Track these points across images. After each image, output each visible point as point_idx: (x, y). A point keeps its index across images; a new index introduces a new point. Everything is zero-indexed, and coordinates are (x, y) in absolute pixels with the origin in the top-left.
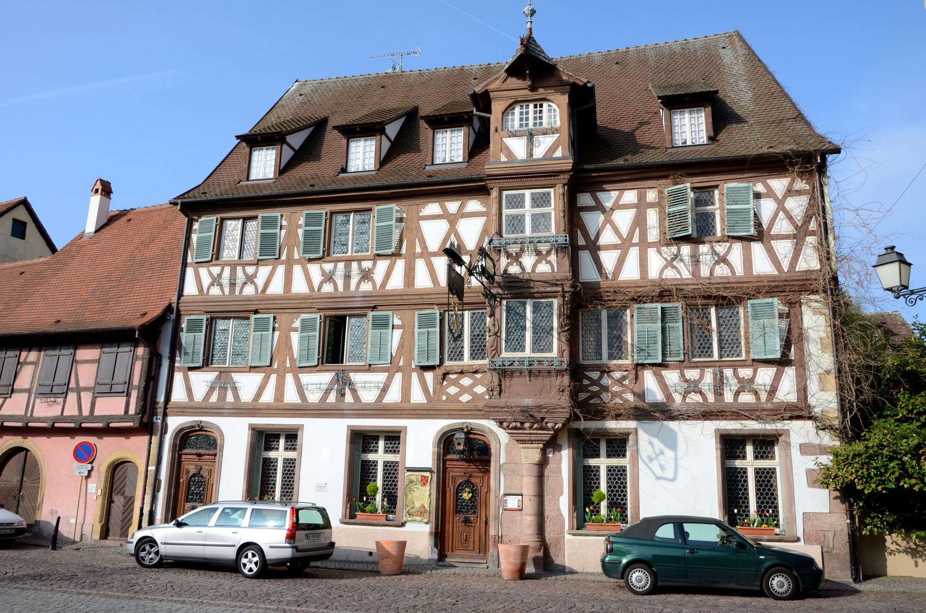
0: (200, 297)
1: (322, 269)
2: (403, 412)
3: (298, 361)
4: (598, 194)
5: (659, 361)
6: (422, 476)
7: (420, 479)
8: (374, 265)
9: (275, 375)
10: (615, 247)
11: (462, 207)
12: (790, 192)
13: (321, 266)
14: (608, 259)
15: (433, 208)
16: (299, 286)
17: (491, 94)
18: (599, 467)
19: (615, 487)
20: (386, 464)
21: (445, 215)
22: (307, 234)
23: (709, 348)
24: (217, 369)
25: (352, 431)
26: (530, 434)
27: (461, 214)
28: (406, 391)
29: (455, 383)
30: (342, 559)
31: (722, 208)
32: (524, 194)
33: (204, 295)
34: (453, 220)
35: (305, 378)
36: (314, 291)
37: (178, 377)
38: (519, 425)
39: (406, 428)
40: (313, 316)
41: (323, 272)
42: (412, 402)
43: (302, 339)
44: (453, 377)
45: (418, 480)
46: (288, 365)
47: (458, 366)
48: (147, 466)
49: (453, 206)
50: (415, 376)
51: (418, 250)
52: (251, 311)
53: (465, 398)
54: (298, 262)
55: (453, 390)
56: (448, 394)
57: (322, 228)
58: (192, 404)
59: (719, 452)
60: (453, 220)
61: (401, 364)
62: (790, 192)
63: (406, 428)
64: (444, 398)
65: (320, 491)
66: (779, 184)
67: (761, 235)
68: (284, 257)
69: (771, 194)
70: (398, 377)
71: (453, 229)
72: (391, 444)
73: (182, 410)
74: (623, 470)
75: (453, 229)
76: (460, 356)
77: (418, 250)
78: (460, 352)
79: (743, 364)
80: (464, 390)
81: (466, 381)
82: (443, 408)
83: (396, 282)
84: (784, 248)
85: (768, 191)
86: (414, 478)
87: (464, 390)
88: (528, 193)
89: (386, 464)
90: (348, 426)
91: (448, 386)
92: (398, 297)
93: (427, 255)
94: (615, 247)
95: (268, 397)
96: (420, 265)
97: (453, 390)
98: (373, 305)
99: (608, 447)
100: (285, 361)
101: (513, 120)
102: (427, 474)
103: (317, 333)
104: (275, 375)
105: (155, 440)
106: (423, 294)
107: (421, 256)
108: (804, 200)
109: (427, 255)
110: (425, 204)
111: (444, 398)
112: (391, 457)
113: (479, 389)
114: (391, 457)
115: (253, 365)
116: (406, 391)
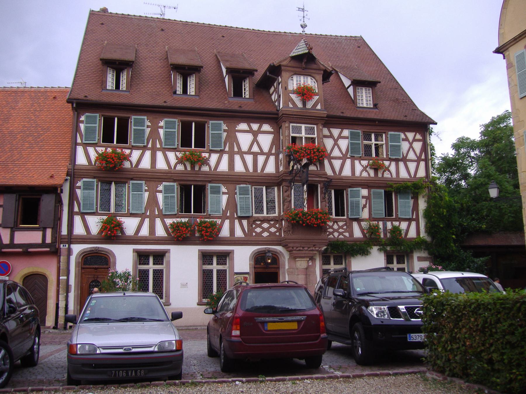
0: (89, 166)
1: (176, 155)
2: (232, 242)
3: (164, 211)
4: (331, 129)
5: (94, 211)
6: (244, 277)
7: (243, 278)
8: (210, 156)
9: (148, 219)
10: (339, 158)
11: (260, 127)
12: (414, 140)
13: (175, 154)
14: (337, 164)
15: (243, 126)
16: (161, 164)
17: (282, 67)
18: (149, 270)
19: (158, 279)
20: (155, 271)
21: (251, 131)
22: (166, 134)
23: (257, 209)
24: (107, 215)
25: (201, 252)
26: (305, 253)
27: (259, 132)
28: (232, 230)
29: (260, 226)
30: (191, 325)
31: (387, 144)
32: (301, 127)
33: (92, 165)
34: (255, 134)
35: (89, 218)
36: (172, 169)
37: (77, 220)
38: (301, 249)
39: (233, 250)
40: (172, 184)
41: (177, 158)
42: (236, 236)
43: (165, 198)
44: (258, 223)
45: (242, 279)
46: (157, 213)
47: (262, 217)
48: (59, 276)
49: (255, 127)
50: (237, 222)
51: (236, 149)
52: (129, 178)
53: (265, 234)
54: (159, 149)
55: (258, 230)
56: (256, 232)
57: (176, 130)
58: (232, 238)
59: (386, 261)
60: (255, 134)
61: (228, 215)
62: (414, 140)
63: (233, 250)
64: (254, 234)
65: (183, 287)
66: (410, 135)
67: (405, 160)
68: (150, 146)
69: (331, 136)
70: (147, 221)
71: (255, 140)
72: (220, 260)
73: (81, 240)
74: (161, 271)
75: (255, 140)
76: (262, 211)
77: (236, 149)
78: (261, 209)
79: (395, 220)
80: (264, 230)
81: (266, 225)
82: (253, 239)
83: (224, 167)
84: (412, 166)
85: (261, 131)
86: (239, 278)
87: (264, 230)
88: (303, 126)
89: (155, 271)
90: (199, 250)
91: (255, 228)
92: (226, 176)
93: (241, 153)
94: (339, 158)
95: (145, 232)
96: (237, 158)
97: (258, 230)
98: (132, 177)
99: (154, 259)
100: (154, 211)
101: (293, 84)
102: (247, 276)
103: (175, 195)
104: (148, 219)
105: (63, 259)
106: (161, 172)
107: (238, 153)
108: (270, 137)
109: (241, 153)
110: (239, 123)
111: (254, 234)
112: (221, 267)
113: (258, 230)
114: (221, 267)
115: (133, 212)
116: (232, 230)
